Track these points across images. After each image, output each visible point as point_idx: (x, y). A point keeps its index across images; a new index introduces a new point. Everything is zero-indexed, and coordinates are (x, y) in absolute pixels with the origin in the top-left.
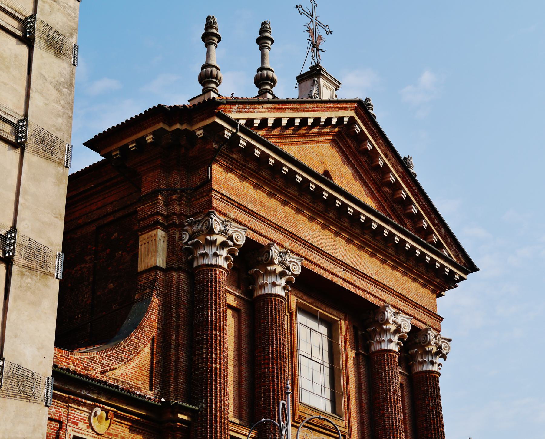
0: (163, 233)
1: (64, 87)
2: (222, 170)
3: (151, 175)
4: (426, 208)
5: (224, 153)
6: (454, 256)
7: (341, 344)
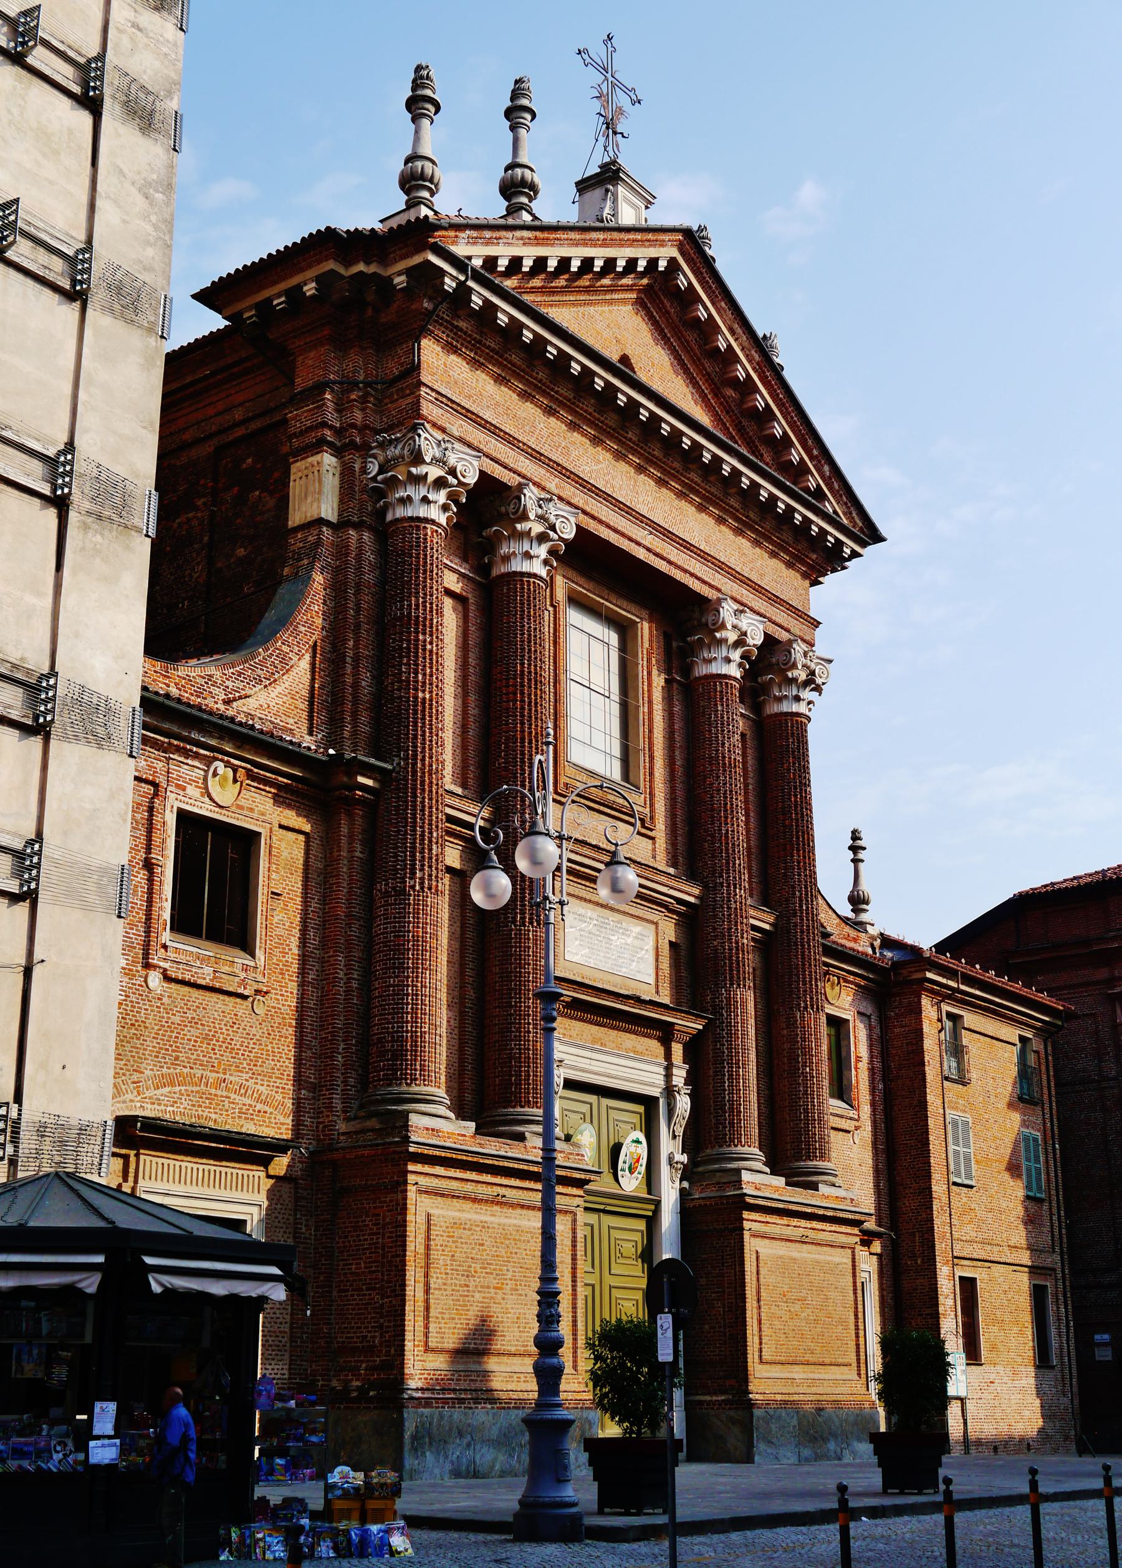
0: (334, 460)
2: (439, 349)
3: (312, 355)
4: (798, 427)
5: (442, 318)
6: (845, 514)
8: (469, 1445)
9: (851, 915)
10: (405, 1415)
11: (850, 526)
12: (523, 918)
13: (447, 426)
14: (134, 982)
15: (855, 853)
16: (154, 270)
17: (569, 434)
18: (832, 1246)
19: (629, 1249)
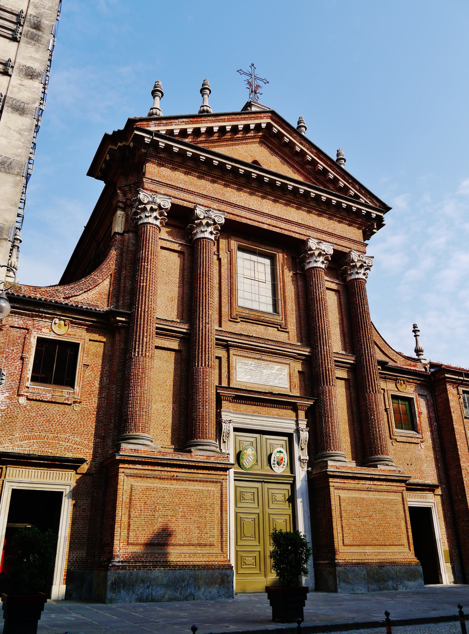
0: (122, 213)
1: (25, 132)
2: (156, 166)
4: (340, 173)
5: (152, 155)
6: (370, 202)
7: (278, 268)
8: (148, 587)
9: (417, 357)
10: (109, 574)
11: (374, 206)
12: (198, 364)
13: (158, 190)
14: (13, 401)
15: (415, 333)
16: (21, 156)
17: (225, 189)
18: (388, 492)
19: (280, 497)
